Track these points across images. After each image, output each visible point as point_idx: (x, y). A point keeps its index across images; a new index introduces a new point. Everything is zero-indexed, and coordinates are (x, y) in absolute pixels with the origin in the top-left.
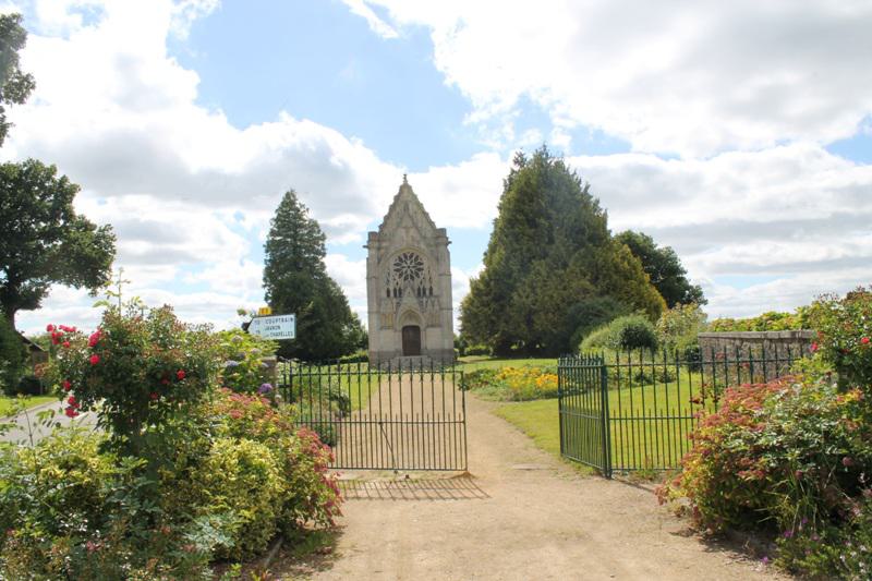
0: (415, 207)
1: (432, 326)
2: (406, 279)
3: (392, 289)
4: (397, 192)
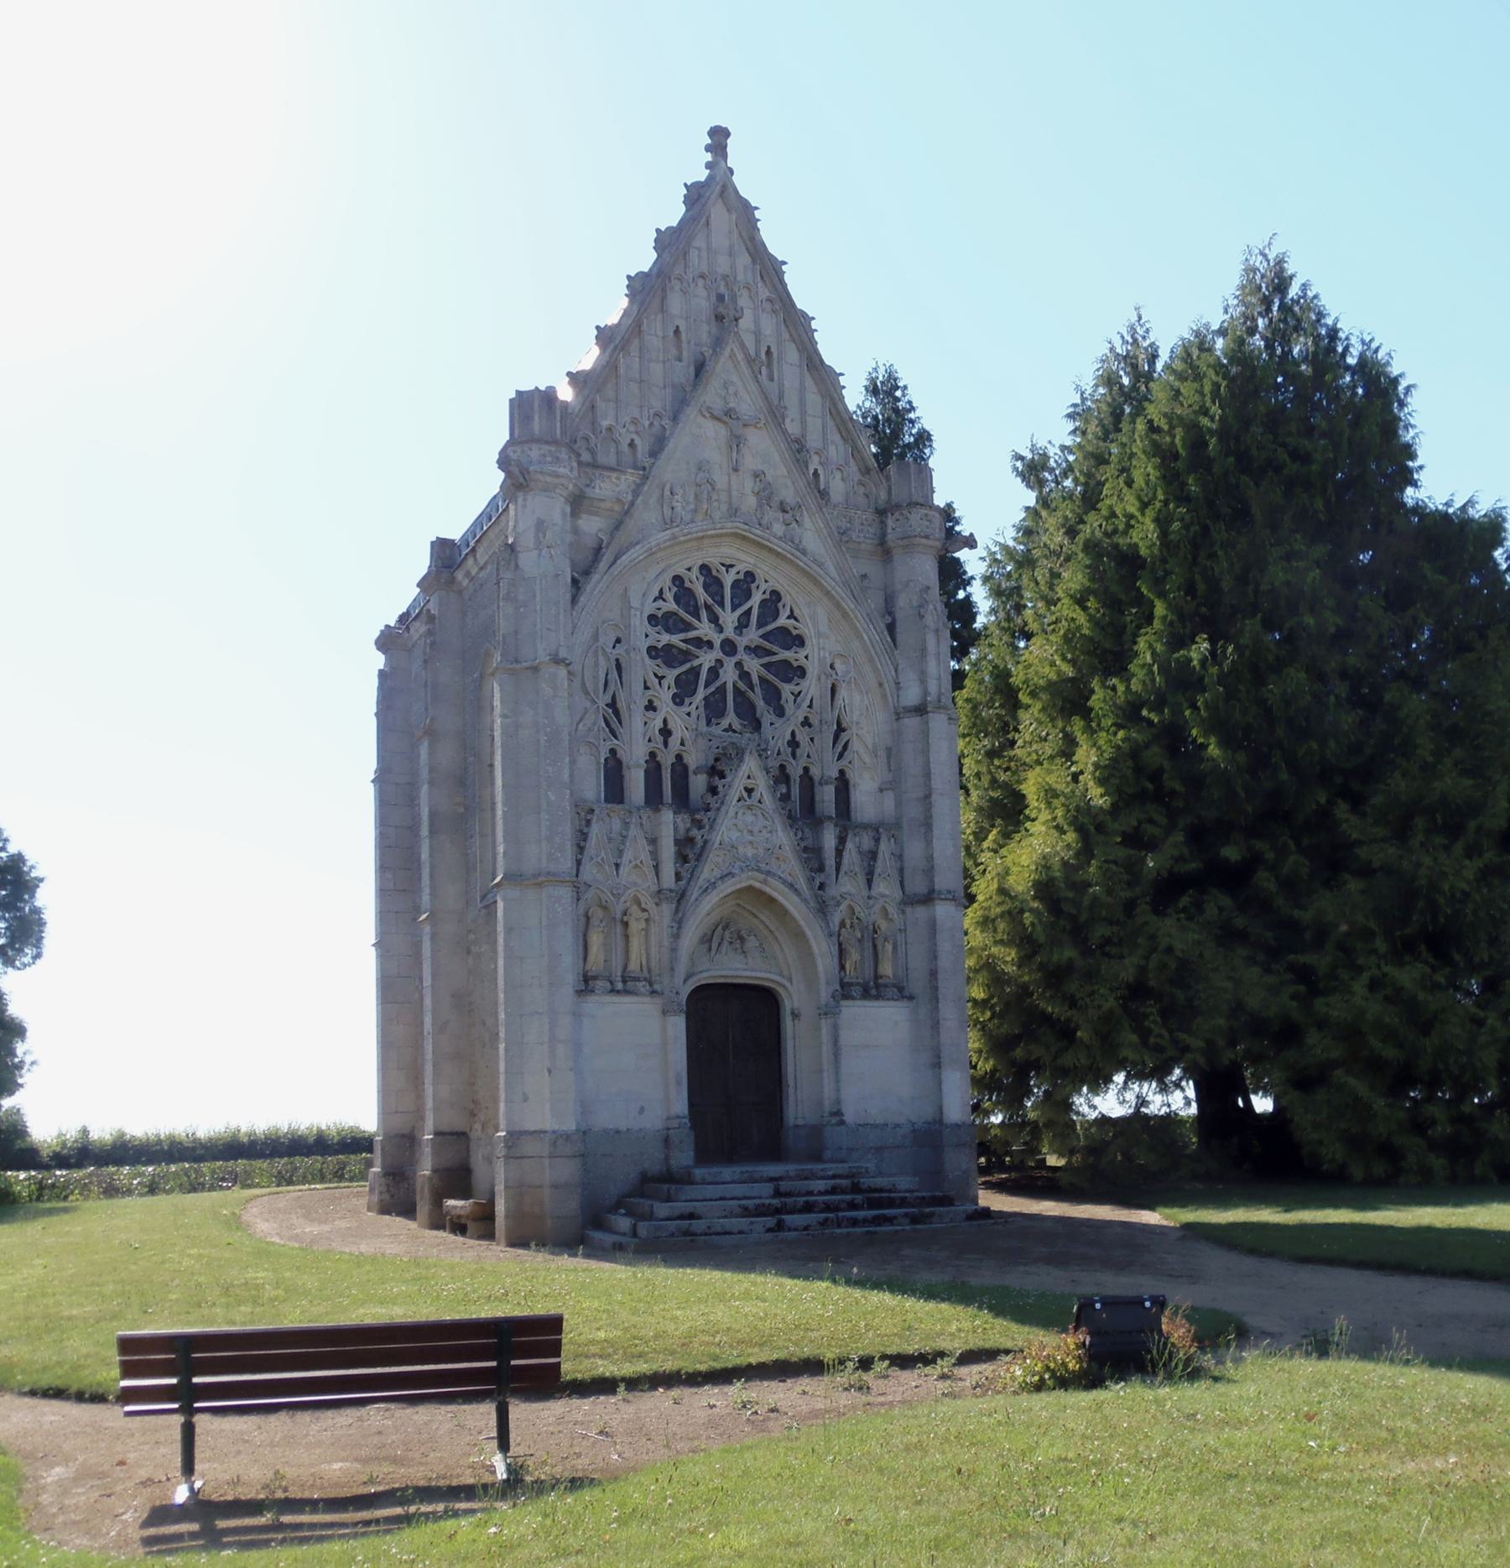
0: (769, 325)
1: (873, 989)
2: (714, 708)
3: (635, 754)
4: (673, 213)
